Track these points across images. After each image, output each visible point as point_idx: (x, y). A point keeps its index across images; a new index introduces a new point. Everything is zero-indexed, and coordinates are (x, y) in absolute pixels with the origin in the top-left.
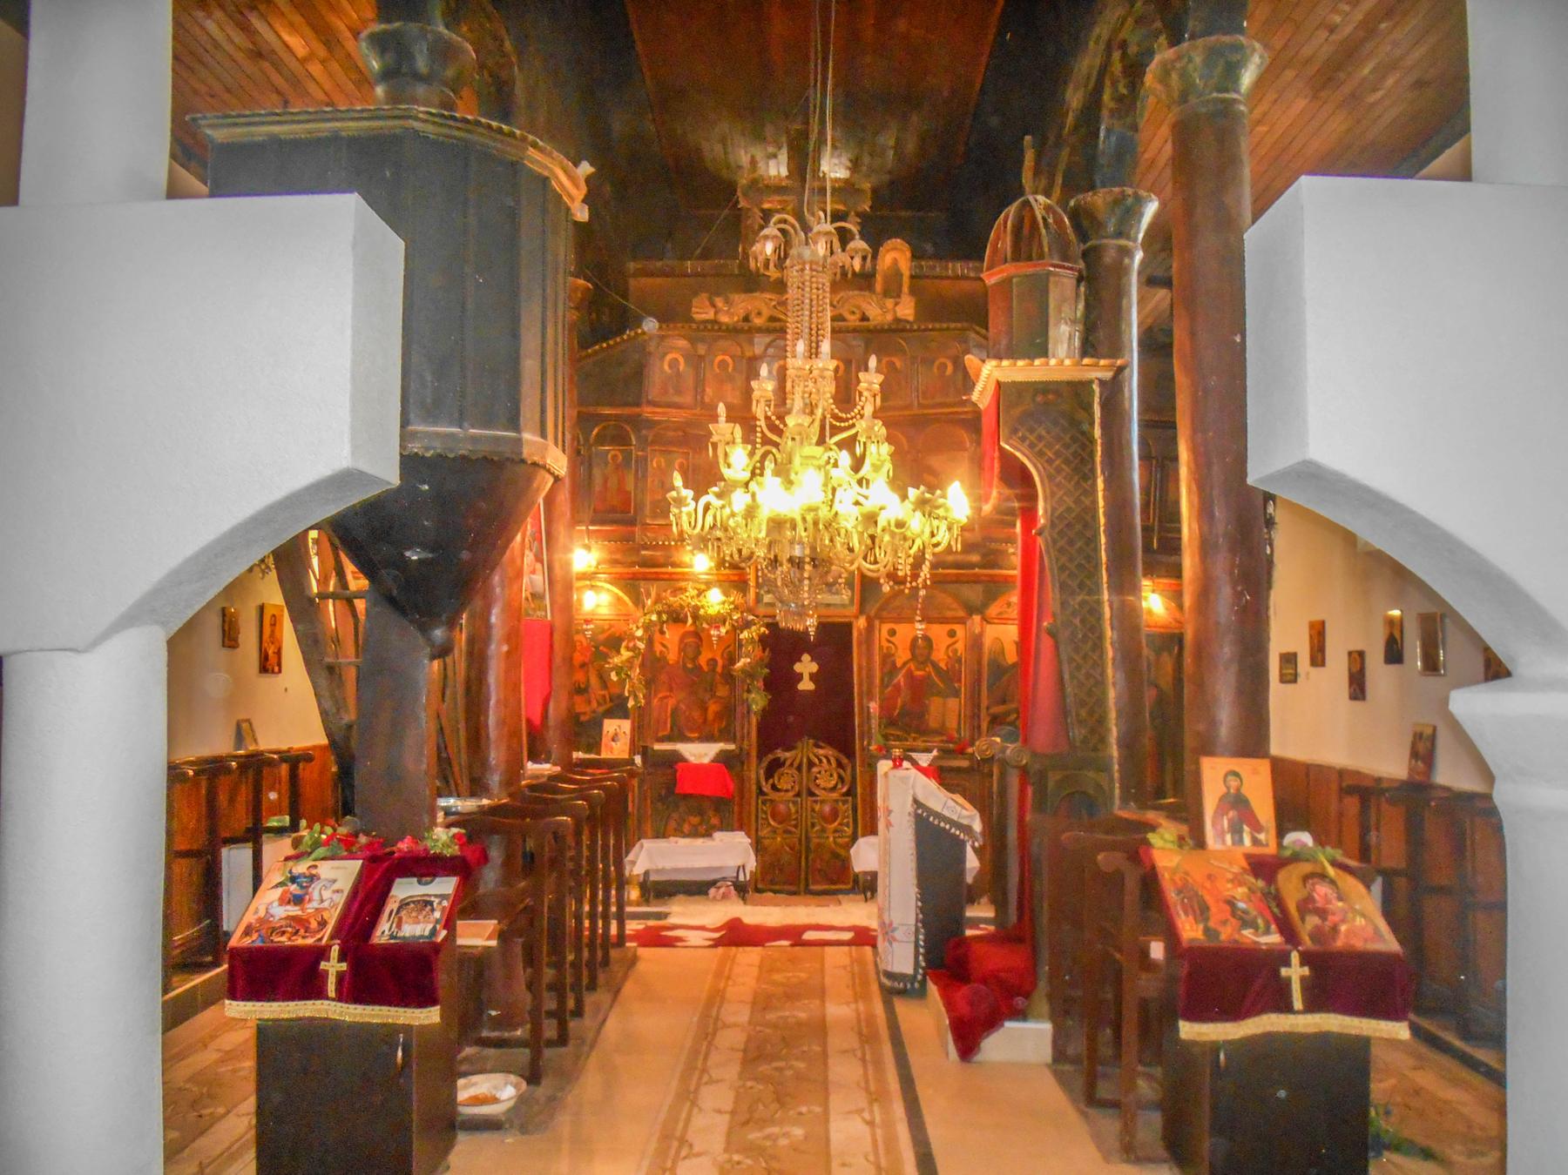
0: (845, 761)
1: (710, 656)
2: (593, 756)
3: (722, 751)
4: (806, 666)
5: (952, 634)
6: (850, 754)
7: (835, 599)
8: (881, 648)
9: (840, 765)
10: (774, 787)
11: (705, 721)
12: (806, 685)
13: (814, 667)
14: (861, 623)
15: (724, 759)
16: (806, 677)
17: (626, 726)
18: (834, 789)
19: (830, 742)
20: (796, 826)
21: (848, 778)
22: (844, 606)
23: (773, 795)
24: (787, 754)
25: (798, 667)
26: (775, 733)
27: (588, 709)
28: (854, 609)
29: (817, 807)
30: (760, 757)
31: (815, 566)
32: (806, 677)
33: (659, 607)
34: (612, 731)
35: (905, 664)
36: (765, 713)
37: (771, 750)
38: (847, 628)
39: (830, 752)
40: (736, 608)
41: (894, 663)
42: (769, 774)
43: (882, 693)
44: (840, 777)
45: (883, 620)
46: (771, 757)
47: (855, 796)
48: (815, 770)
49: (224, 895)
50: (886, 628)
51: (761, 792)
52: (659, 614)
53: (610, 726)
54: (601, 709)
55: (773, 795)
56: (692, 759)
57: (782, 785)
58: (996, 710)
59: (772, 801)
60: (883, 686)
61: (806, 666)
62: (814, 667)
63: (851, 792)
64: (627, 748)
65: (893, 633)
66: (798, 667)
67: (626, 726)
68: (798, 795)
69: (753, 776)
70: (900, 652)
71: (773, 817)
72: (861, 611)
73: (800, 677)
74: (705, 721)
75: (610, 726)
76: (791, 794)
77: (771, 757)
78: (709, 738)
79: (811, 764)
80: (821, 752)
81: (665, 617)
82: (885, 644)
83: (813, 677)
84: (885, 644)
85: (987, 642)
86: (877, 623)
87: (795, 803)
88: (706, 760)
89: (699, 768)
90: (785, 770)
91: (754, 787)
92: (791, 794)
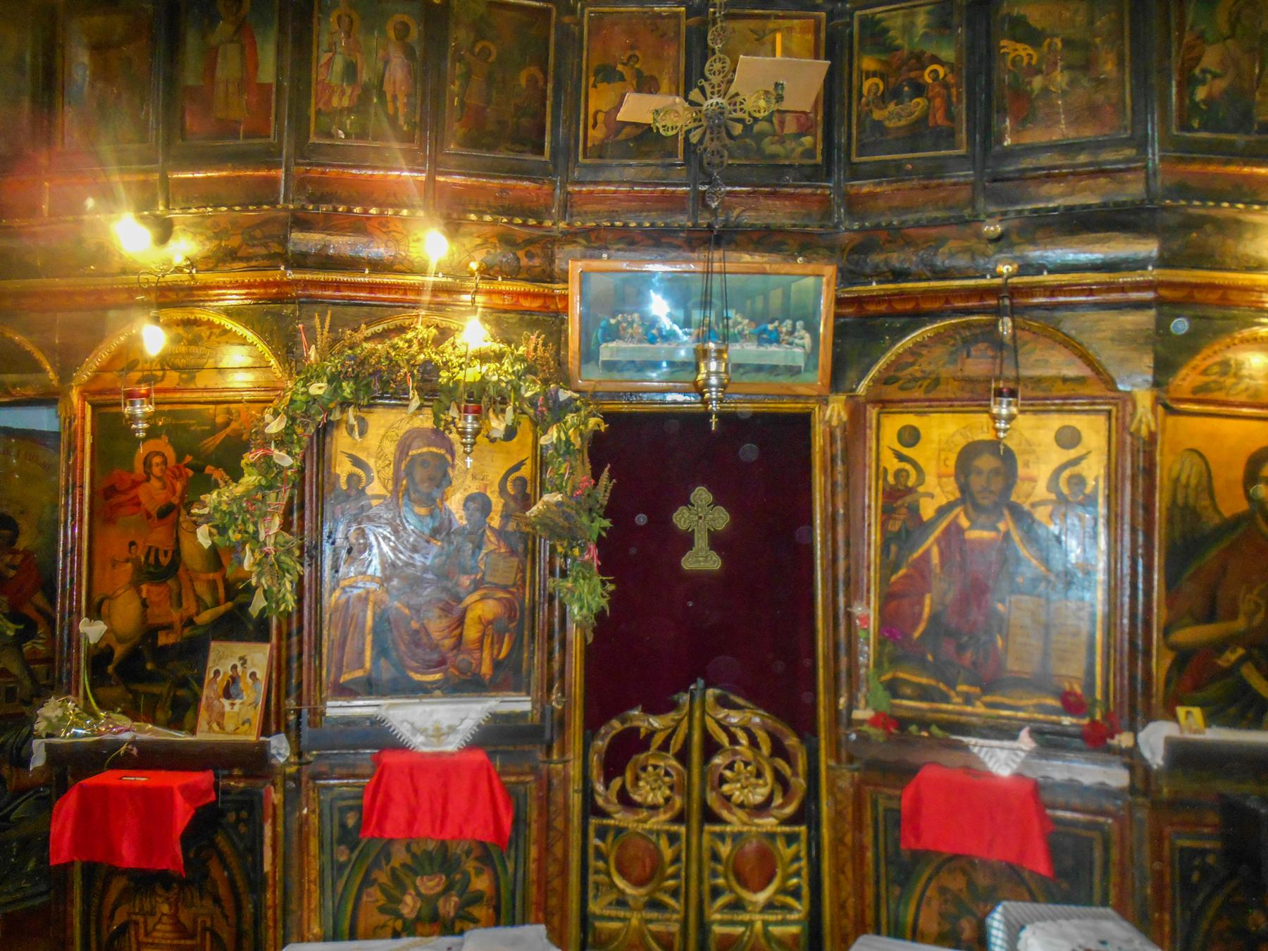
0: (792, 741)
1: (474, 488)
2: (182, 736)
3: (495, 716)
4: (701, 514)
5: (1068, 438)
6: (805, 726)
7: (775, 354)
8: (881, 473)
9: (779, 749)
10: (625, 800)
11: (459, 643)
12: (701, 560)
13: (721, 519)
14: (835, 411)
15: (497, 735)
16: (701, 542)
17: (259, 657)
18: (762, 808)
19: (758, 698)
20: (675, 893)
21: (800, 783)
22: (793, 371)
23: (620, 818)
24: (656, 722)
25: (682, 519)
26: (637, 662)
27: (175, 616)
28: (817, 379)
29: (725, 850)
30: (592, 725)
31: (638, 48)
32: (701, 542)
33: (331, 366)
34: (225, 669)
35: (942, 511)
36: (603, 624)
37: (618, 708)
38: (802, 423)
39: (756, 719)
40: (530, 370)
41: (914, 510)
42: (615, 762)
43: (884, 580)
44: (779, 778)
45: (885, 404)
46: (616, 725)
47: (815, 826)
48: (718, 760)
49: (1098, 235)
50: (893, 424)
51: (591, 808)
52: (334, 379)
53: (225, 658)
54: (205, 617)
55: (620, 818)
56: (420, 744)
57: (647, 792)
58: (1187, 635)
59: (620, 831)
60: (889, 566)
61: (701, 514)
62: (721, 519)
63: (806, 814)
64: (256, 716)
65: (911, 437)
66: (682, 519)
67: (259, 657)
68: (680, 818)
69: (575, 771)
70: (931, 482)
71: (623, 874)
72: (837, 380)
73: (687, 541)
74: (459, 643)
75: (225, 658)
76: (663, 816)
77: (616, 725)
78: (467, 684)
79: (711, 747)
80: (735, 718)
81: (347, 389)
82: (892, 464)
83: (717, 542)
84: (892, 464)
85: (1167, 464)
86: (872, 412)
87: (673, 838)
88: (452, 745)
89: (442, 767)
90: (646, 757)
91: (576, 800)
92: (663, 816)
